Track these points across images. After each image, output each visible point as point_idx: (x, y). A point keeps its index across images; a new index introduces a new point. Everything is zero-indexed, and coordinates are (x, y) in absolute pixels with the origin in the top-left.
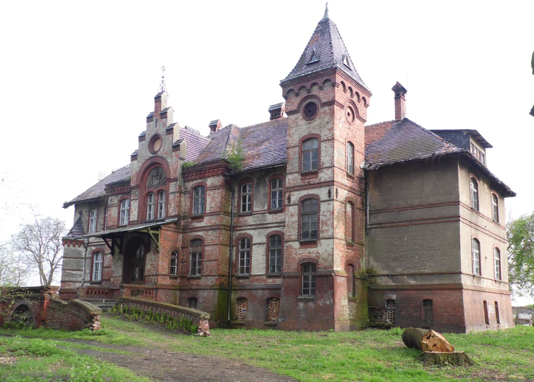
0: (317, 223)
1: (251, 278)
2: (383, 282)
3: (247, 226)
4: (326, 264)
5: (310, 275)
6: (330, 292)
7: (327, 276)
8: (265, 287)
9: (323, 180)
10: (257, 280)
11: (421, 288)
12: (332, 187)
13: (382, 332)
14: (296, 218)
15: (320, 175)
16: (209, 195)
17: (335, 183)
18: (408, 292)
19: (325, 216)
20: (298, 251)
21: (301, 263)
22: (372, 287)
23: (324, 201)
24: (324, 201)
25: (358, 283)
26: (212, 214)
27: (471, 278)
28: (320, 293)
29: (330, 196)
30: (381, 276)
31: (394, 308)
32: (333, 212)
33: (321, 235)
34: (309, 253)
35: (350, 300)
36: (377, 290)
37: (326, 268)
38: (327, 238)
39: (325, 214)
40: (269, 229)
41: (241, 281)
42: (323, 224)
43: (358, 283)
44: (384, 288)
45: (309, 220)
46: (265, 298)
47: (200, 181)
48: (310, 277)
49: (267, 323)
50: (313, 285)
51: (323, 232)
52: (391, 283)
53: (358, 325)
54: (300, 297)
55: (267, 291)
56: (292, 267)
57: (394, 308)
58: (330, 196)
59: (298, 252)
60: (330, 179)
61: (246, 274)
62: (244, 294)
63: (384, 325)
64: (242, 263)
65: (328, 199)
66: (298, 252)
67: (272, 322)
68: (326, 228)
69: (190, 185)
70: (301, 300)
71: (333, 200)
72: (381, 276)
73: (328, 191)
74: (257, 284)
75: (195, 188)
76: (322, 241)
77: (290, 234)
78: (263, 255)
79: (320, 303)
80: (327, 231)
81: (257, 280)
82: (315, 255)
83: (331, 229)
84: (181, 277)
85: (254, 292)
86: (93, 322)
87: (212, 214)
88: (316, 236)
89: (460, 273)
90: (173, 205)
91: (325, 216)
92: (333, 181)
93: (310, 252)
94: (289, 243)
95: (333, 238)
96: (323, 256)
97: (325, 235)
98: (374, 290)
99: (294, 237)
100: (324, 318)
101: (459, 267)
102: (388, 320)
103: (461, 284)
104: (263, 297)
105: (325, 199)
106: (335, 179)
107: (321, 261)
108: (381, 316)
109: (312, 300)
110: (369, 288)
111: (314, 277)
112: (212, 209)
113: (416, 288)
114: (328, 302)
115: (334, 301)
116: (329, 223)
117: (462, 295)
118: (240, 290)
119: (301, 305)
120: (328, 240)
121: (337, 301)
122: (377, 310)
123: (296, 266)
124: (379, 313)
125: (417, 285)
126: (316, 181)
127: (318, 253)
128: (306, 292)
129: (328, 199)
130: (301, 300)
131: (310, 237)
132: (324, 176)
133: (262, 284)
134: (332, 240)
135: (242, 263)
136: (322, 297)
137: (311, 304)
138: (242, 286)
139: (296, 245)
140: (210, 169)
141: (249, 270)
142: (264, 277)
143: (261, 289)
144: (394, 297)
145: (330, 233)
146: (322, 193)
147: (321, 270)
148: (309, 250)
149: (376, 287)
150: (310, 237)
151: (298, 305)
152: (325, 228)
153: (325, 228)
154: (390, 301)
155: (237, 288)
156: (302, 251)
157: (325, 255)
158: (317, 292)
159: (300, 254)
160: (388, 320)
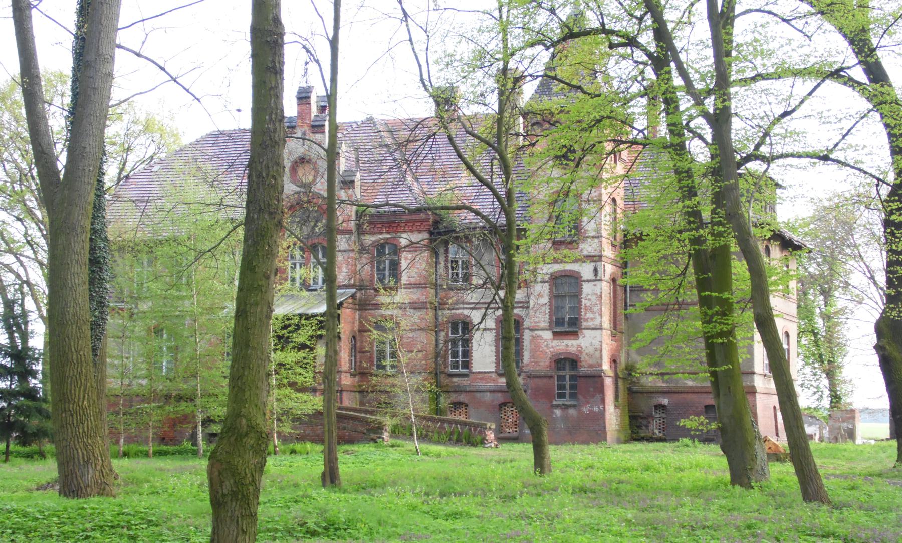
0: (577, 308)
1: (472, 376)
2: (650, 381)
3: (463, 304)
4: (591, 362)
5: (567, 373)
6: (598, 396)
7: (594, 376)
8: (496, 388)
9: (585, 253)
10: (481, 379)
11: (703, 390)
12: (599, 263)
13: (661, 444)
14: (545, 300)
15: (582, 246)
16: (406, 259)
17: (603, 259)
18: (685, 396)
19: (590, 300)
20: (550, 342)
21: (554, 359)
22: (635, 388)
23: (588, 281)
24: (588, 281)
25: (620, 383)
26: (409, 286)
27: (762, 377)
28: (585, 397)
29: (596, 275)
30: (479, 138)
31: (664, 415)
32: (601, 296)
33: (584, 324)
34: (567, 346)
35: (616, 406)
36: (642, 393)
37: (591, 366)
38: (593, 329)
39: (589, 297)
40: (676, 395)
41: (455, 379)
42: (586, 310)
43: (620, 383)
44: (652, 390)
45: (568, 304)
46: (497, 403)
47: (389, 236)
48: (568, 377)
49: (502, 435)
50: (572, 387)
51: (586, 320)
52: (660, 384)
53: (623, 438)
54: (554, 402)
55: (499, 394)
56: (542, 364)
57: (664, 415)
58: (596, 275)
59: (551, 344)
60: (596, 253)
61: (461, 370)
62: (462, 398)
63: (652, 438)
64: (455, 355)
65: (594, 278)
66: (551, 344)
67: (507, 435)
68: (592, 316)
69: (369, 239)
70: (557, 406)
71: (601, 280)
72: (479, 138)
73: (593, 268)
74: (482, 385)
75: (380, 247)
76: (585, 332)
77: (537, 320)
78: (490, 345)
79: (586, 410)
80: (592, 319)
81: (481, 379)
82: (575, 349)
83: (599, 318)
84: (360, 373)
85: (478, 395)
86: (382, 433)
87: (409, 286)
88: (575, 324)
89: (753, 373)
90: (344, 270)
91: (590, 300)
92: (601, 256)
93: (568, 345)
94: (536, 332)
95: (601, 329)
96: (587, 351)
97: (590, 324)
98: (637, 392)
99: (544, 324)
100: (592, 428)
101: (752, 365)
102: (657, 431)
103: (754, 387)
104: (493, 401)
105: (589, 278)
106: (603, 253)
107: (584, 357)
108: (647, 426)
109: (574, 406)
110: (629, 389)
111: (572, 378)
112: (412, 280)
113: (696, 390)
114: (596, 409)
115: (604, 408)
116: (595, 309)
117: (755, 401)
118: (455, 391)
119: (558, 412)
120: (594, 332)
121: (607, 407)
122: (642, 418)
123: (547, 363)
124: (644, 422)
125: (696, 387)
126: (576, 253)
127: (579, 346)
128: (561, 396)
129: (594, 278)
130: (557, 406)
131: (567, 324)
132: (587, 248)
133: (490, 385)
134: (599, 331)
135: (455, 355)
136: (588, 403)
137: (572, 411)
138: (458, 386)
139: (547, 335)
140: (408, 221)
141: (467, 365)
142: (494, 375)
143: (490, 391)
144: (665, 401)
145: (597, 323)
146: (586, 270)
147: (584, 369)
148: (566, 342)
149: (640, 389)
150: (566, 326)
151: (553, 413)
152: (589, 315)
153: (589, 315)
154: (660, 407)
155: (450, 389)
156: (556, 343)
157: (591, 350)
158: (580, 397)
159: (553, 347)
160: (657, 431)
